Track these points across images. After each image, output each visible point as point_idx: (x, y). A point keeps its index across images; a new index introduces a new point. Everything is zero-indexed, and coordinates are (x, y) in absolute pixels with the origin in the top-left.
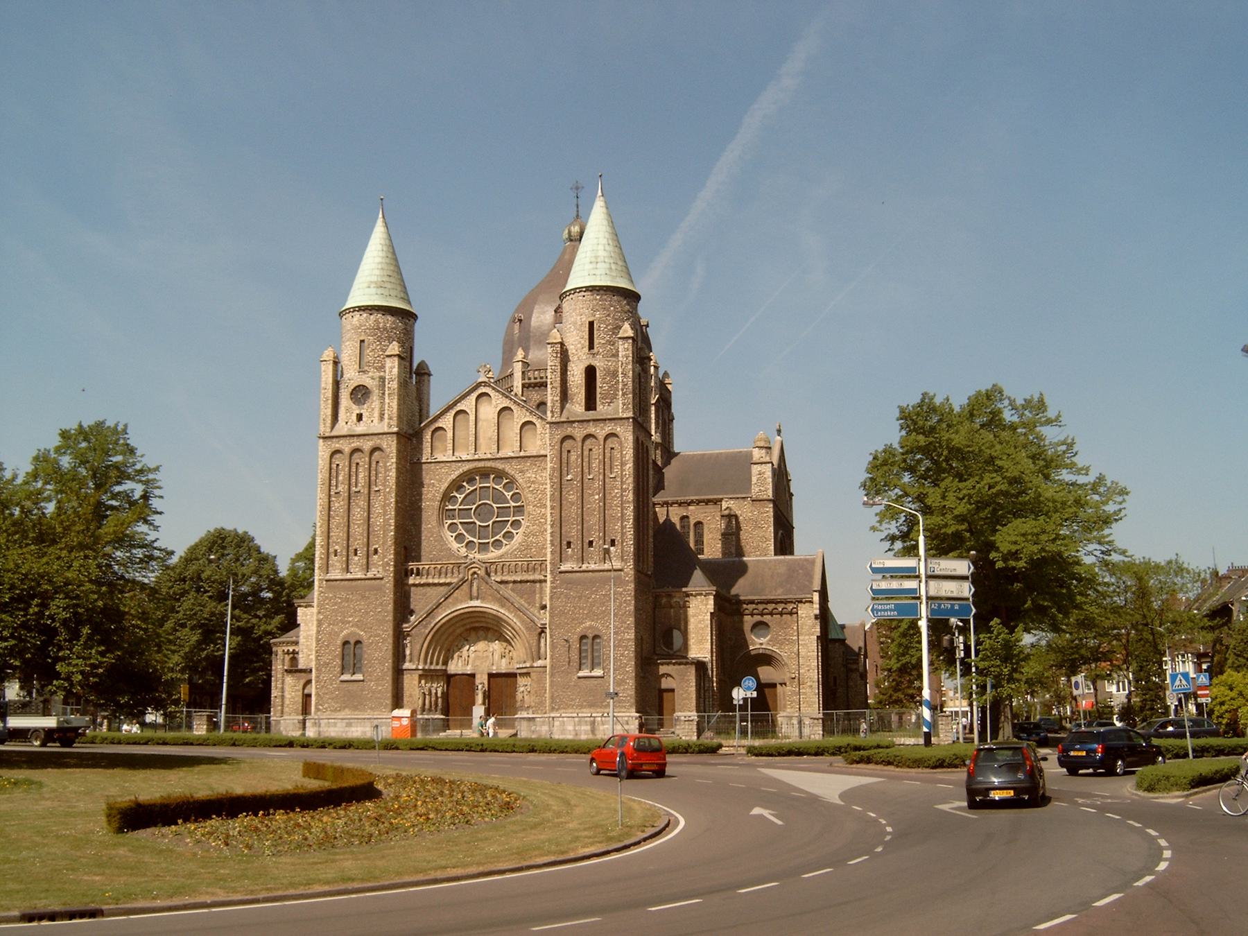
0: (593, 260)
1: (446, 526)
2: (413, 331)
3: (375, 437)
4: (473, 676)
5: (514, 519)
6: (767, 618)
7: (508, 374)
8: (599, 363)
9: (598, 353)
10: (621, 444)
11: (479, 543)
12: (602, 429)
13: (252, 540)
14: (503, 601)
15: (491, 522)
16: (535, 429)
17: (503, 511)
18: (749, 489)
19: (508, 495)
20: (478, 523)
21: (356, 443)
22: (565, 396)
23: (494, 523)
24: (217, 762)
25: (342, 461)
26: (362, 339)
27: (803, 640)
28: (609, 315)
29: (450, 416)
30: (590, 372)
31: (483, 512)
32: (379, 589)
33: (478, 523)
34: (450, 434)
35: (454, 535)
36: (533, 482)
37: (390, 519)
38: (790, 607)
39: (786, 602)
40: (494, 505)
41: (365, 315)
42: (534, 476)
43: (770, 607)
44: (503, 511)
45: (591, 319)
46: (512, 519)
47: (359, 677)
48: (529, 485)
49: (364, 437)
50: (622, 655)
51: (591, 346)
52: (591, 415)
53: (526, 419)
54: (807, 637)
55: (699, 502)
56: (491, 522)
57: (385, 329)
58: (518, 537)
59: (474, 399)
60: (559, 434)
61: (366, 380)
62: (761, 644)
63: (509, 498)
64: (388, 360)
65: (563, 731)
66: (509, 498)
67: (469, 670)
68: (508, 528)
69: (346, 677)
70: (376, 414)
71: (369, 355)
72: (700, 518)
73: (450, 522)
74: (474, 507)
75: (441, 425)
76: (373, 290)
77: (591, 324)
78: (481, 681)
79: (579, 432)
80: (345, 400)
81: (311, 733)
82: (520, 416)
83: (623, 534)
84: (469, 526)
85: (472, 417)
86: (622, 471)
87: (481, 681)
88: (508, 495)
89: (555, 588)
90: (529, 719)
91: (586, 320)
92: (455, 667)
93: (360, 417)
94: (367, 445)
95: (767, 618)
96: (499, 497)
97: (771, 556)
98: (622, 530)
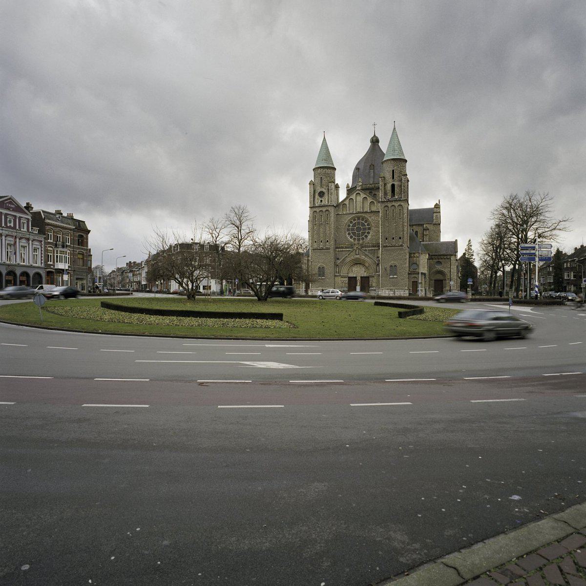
2: (334, 175)
4: (356, 277)
6: (441, 260)
8: (396, 183)
9: (395, 180)
10: (402, 208)
14: (366, 255)
16: (374, 204)
17: (365, 229)
18: (433, 221)
21: (321, 209)
22: (385, 194)
24: (462, 301)
25: (317, 216)
29: (348, 200)
30: (393, 186)
32: (329, 252)
34: (348, 205)
39: (447, 255)
43: (442, 257)
44: (365, 229)
51: (393, 178)
55: (416, 225)
58: (369, 237)
60: (383, 205)
61: (323, 190)
65: (385, 293)
67: (355, 276)
68: (366, 234)
69: (391, 277)
70: (327, 200)
71: (324, 182)
72: (417, 230)
77: (393, 171)
78: (359, 278)
79: (389, 205)
80: (317, 196)
81: (310, 294)
83: (403, 236)
85: (355, 201)
87: (359, 278)
90: (374, 290)
91: (391, 169)
92: (351, 275)
93: (321, 201)
95: (441, 260)
96: (363, 225)
97: (458, 239)
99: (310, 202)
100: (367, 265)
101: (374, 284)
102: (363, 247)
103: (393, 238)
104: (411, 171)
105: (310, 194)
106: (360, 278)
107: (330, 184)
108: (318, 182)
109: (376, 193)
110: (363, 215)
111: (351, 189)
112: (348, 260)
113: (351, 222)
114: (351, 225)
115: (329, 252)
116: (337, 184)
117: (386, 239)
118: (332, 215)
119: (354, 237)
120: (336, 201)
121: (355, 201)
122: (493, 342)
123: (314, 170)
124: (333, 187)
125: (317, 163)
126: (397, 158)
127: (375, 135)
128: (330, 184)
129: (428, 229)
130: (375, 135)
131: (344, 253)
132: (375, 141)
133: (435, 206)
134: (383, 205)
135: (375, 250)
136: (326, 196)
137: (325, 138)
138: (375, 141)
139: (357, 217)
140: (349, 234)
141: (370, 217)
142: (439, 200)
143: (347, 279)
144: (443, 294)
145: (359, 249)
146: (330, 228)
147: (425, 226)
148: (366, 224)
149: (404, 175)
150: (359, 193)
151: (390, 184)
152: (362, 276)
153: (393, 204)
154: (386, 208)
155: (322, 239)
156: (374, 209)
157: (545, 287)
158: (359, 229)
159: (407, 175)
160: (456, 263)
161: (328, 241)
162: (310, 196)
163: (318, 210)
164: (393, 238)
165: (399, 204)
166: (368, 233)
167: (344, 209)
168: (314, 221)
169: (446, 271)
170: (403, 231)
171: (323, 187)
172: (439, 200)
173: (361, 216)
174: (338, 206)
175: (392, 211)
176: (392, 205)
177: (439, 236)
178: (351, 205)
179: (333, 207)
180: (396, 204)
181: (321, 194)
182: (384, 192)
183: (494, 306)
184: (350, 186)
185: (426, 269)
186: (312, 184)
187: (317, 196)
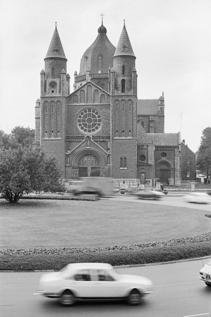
1: (78, 124)
3: (58, 98)
5: (98, 123)
6: (165, 152)
7: (83, 75)
10: (132, 103)
11: (88, 130)
12: (127, 98)
13: (19, 127)
15: (91, 124)
17: (95, 121)
19: (97, 116)
20: (88, 124)
23: (92, 124)
27: (176, 158)
30: (123, 81)
31: (90, 120)
33: (88, 124)
35: (80, 127)
36: (104, 112)
37: (63, 122)
38: (172, 149)
40: (92, 119)
42: (104, 110)
44: (95, 121)
46: (98, 123)
47: (126, 168)
48: (103, 113)
49: (55, 98)
50: (133, 163)
51: (123, 73)
52: (124, 94)
53: (102, 94)
54: (177, 157)
56: (91, 124)
59: (86, 87)
62: (164, 159)
63: (97, 117)
64: (62, 75)
66: (97, 117)
68: (97, 125)
73: (79, 123)
74: (86, 119)
75: (76, 94)
77: (123, 67)
84: (85, 125)
85: (86, 92)
86: (133, 111)
88: (97, 116)
89: (113, 144)
93: (53, 92)
94: (56, 100)
96: (94, 117)
98: (133, 128)
99: (42, 92)
103: (123, 131)
104: (139, 66)
108: (49, 71)
109: (104, 83)
114: (82, 116)
119: (85, 128)
121: (86, 92)
122: (69, 307)
123: (45, 59)
124: (65, 78)
126: (127, 55)
127: (102, 25)
130: (102, 25)
132: (102, 31)
137: (56, 29)
138: (102, 31)
140: (80, 125)
142: (163, 92)
143: (78, 170)
146: (61, 119)
147: (150, 117)
148: (85, 114)
149: (133, 72)
150: (90, 85)
154: (117, 102)
155: (53, 130)
158: (90, 120)
159: (136, 72)
162: (42, 86)
164: (123, 131)
166: (99, 125)
170: (133, 125)
172: (163, 92)
174: (71, 97)
175: (122, 105)
176: (115, 99)
177: (192, 153)
179: (64, 98)
181: (53, 85)
182: (115, 87)
183: (95, 178)
184: (78, 74)
186: (43, 74)
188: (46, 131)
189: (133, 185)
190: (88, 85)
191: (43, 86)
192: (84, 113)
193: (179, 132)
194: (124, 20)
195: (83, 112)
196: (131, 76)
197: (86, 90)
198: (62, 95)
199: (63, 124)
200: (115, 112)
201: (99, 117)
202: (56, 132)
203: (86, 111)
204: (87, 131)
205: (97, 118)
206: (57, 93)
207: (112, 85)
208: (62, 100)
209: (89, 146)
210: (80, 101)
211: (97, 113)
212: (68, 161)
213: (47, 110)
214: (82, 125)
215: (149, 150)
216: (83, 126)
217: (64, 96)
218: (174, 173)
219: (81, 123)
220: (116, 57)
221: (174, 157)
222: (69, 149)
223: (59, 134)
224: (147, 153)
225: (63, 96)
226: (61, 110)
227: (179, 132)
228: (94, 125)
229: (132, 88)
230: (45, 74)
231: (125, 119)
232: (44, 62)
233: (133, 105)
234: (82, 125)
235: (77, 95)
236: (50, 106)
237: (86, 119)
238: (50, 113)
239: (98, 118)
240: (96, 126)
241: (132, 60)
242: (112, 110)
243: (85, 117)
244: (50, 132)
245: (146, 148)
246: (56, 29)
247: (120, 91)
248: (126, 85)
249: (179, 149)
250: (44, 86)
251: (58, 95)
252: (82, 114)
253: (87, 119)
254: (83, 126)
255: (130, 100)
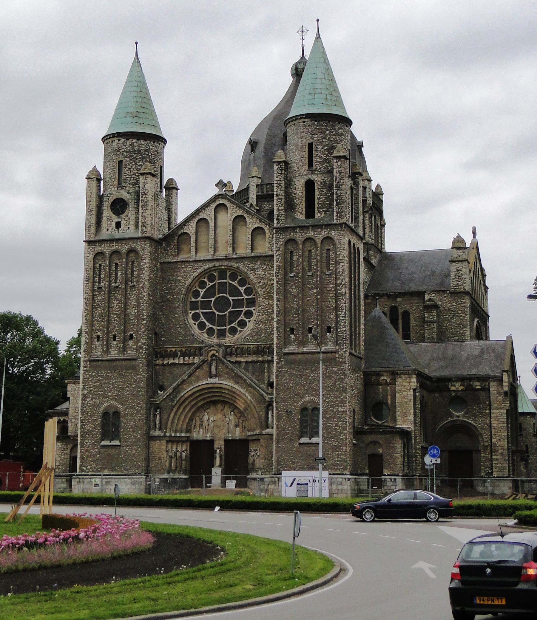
0: (312, 91)
1: (190, 315)
5: (247, 309)
8: (317, 178)
10: (334, 245)
14: (237, 379)
17: (238, 303)
20: (217, 313)
21: (115, 247)
22: (290, 206)
23: (229, 312)
25: (104, 263)
26: (120, 160)
28: (325, 138)
30: (309, 185)
31: (222, 304)
32: (134, 368)
34: (193, 239)
36: (262, 278)
37: (143, 310)
40: (230, 298)
41: (123, 140)
42: (263, 273)
44: (238, 303)
45: (310, 141)
46: (245, 309)
48: (259, 280)
51: (310, 164)
52: (310, 221)
56: (227, 312)
57: (139, 151)
58: (250, 325)
59: (213, 210)
61: (124, 195)
62: (458, 417)
66: (242, 292)
67: (208, 437)
68: (242, 317)
70: (132, 222)
73: (193, 312)
74: (213, 299)
76: (129, 119)
77: (310, 145)
78: (219, 445)
79: (300, 237)
80: (107, 212)
82: (252, 223)
83: (337, 322)
84: (210, 317)
85: (212, 225)
87: (219, 445)
91: (306, 142)
92: (198, 434)
93: (118, 225)
94: (124, 248)
96: (234, 292)
99: (88, 228)
100: (241, 405)
101: (259, 463)
102: (231, 354)
105: (88, 206)
106: (222, 443)
107: (142, 180)
110: (234, 265)
111: (237, 193)
112: (187, 390)
113: (202, 285)
114: (202, 292)
115: (134, 368)
116: (171, 181)
117: (292, 330)
118: (146, 262)
119: (209, 325)
120: (166, 225)
121: (212, 225)
123: (104, 139)
125: (112, 125)
128: (142, 180)
129: (436, 307)
131: (177, 371)
133: (453, 243)
134: (284, 237)
135: (263, 362)
136: (131, 212)
137: (137, 58)
139: (216, 269)
140: (196, 317)
141: (253, 269)
142: (474, 228)
144: (246, 487)
145: (218, 360)
146: (137, 299)
147: (427, 297)
148: (242, 289)
151: (303, 181)
152: (230, 437)
153: (311, 234)
154: (291, 247)
156: (263, 248)
157: (79, 472)
158: (222, 304)
160: (504, 401)
161: (131, 337)
162: (89, 211)
163: (107, 249)
165: (325, 233)
166: (249, 314)
167: (184, 247)
168: (97, 279)
169: (478, 424)
171: (123, 188)
172: (474, 228)
173: (229, 268)
176: (288, 237)
178: (202, 238)
179: (147, 242)
180: (319, 236)
185: (412, 418)
187: (107, 212)
188: (98, 337)
189: (340, 492)
190: (218, 203)
191: (92, 211)
192: (208, 283)
193: (510, 338)
194: (318, 21)
195: (206, 280)
196: (330, 172)
197: (213, 218)
198: (143, 232)
199: (143, 315)
200: (286, 273)
201: (249, 291)
202: (124, 336)
203: (211, 278)
204: (215, 335)
205: (243, 296)
206: (129, 228)
207: (278, 199)
208: (141, 248)
209: (216, 376)
210: (196, 249)
211: (242, 282)
212: (157, 422)
213: (102, 276)
214: (202, 316)
215: (398, 388)
216: (204, 320)
217: (147, 235)
218: (491, 460)
219: (198, 311)
220: (296, 120)
221: (490, 410)
222: (162, 388)
223: (131, 342)
224: (394, 397)
225: (144, 235)
226: (139, 275)
227: (510, 338)
228: (235, 315)
229: (335, 203)
230: (99, 180)
231: (315, 293)
232: (102, 146)
233: (338, 253)
234: (202, 316)
235: (187, 233)
236: (110, 266)
237: (213, 299)
238: (110, 285)
239: (246, 297)
240: (239, 319)
241: (337, 128)
242: (278, 267)
243: (209, 293)
244: (108, 337)
245: (388, 381)
246: (137, 58)
247: (301, 213)
248: (319, 196)
249: (502, 386)
250: (94, 212)
251: (131, 232)
252: (202, 285)
253: (215, 300)
254: (204, 320)
255: (328, 239)
